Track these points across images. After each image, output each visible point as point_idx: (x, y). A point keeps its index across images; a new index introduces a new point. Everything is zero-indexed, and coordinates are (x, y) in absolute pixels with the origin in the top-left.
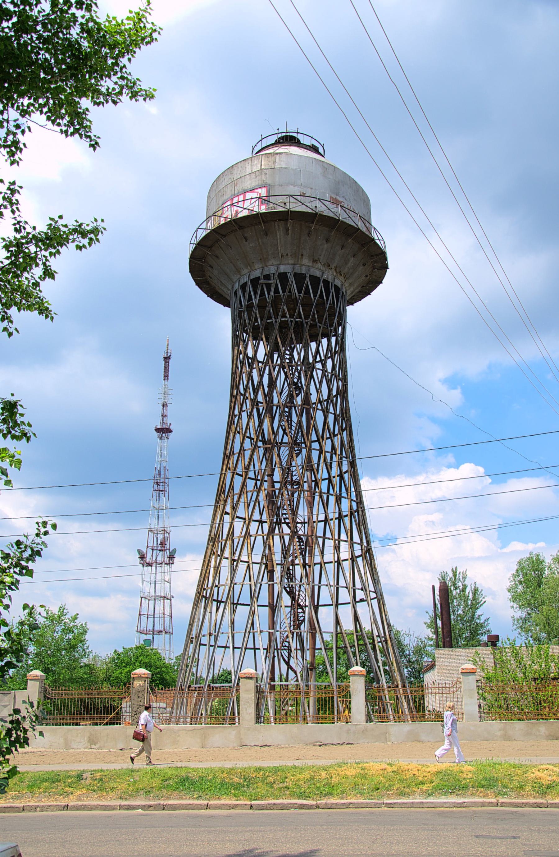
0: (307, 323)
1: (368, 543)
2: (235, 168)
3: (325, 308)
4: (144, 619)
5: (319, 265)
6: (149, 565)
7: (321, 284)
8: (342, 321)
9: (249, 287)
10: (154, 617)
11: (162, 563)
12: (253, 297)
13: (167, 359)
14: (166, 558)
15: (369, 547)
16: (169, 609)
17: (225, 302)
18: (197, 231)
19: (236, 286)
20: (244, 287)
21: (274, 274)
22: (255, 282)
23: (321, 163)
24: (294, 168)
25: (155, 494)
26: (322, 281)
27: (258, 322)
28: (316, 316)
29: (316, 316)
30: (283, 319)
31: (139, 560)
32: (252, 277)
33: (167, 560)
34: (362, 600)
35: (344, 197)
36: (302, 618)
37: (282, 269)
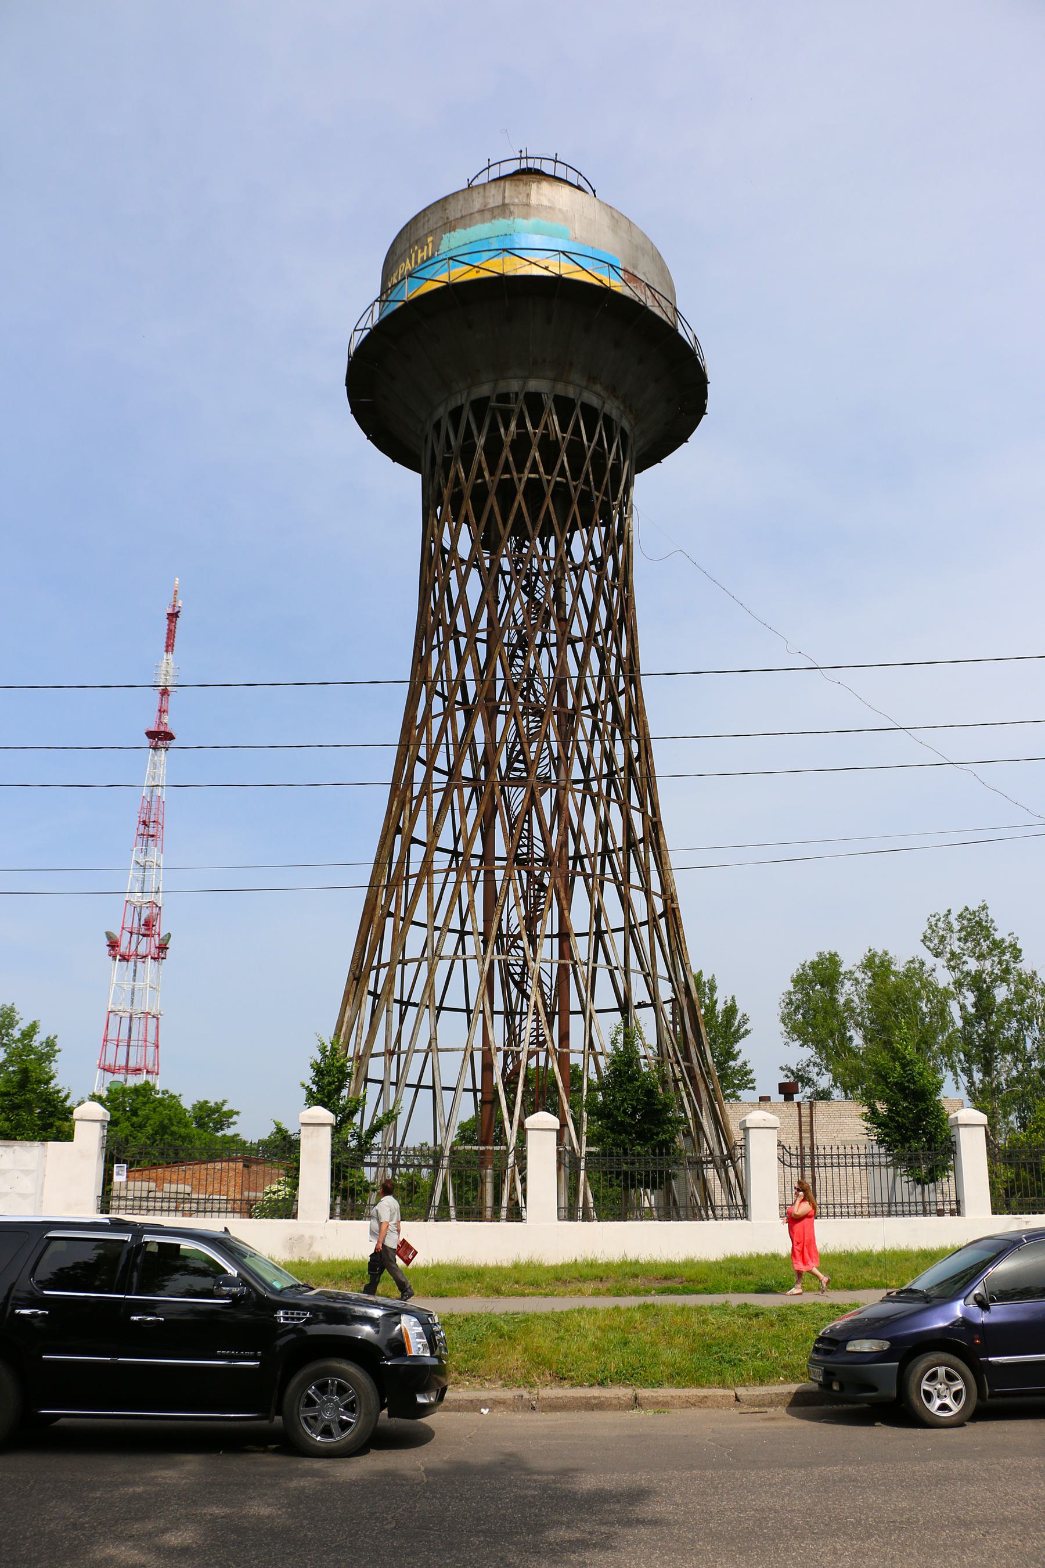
0: (575, 487)
2: (451, 199)
3: (606, 465)
4: (111, 1047)
5: (598, 388)
6: (125, 958)
9: (467, 414)
10: (129, 1046)
12: (475, 432)
13: (173, 616)
14: (153, 949)
16: (154, 1034)
19: (442, 412)
20: (456, 415)
21: (517, 394)
22: (479, 406)
23: (609, 209)
25: (140, 840)
30: (532, 476)
31: (108, 949)
32: (473, 397)
33: (154, 951)
37: (534, 385)
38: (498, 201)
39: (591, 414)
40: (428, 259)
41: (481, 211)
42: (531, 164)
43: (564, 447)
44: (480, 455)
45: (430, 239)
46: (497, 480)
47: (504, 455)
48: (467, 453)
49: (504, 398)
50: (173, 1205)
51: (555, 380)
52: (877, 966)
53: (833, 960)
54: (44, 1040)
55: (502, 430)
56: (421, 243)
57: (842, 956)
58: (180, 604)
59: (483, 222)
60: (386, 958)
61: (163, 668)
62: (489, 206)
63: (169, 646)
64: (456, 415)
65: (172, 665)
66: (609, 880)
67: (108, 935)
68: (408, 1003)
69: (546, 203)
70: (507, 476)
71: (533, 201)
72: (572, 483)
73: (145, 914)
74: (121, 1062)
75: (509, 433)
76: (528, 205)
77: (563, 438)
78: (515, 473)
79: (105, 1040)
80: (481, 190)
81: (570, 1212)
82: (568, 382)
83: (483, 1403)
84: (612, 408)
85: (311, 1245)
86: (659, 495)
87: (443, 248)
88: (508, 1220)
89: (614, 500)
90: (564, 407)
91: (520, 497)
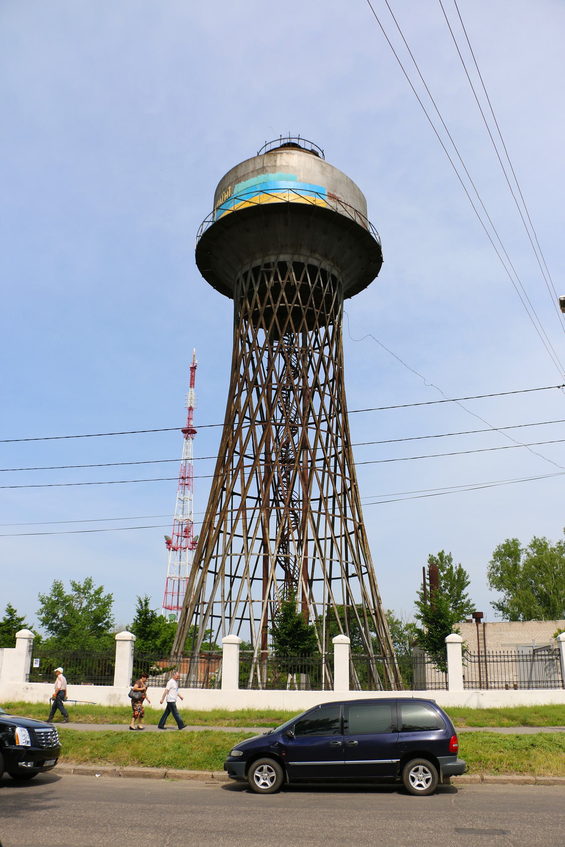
0: (304, 309)
1: (360, 520)
2: (239, 167)
3: (322, 295)
4: (169, 596)
5: (317, 256)
6: (175, 549)
7: (319, 273)
8: (337, 311)
9: (251, 275)
10: (178, 595)
11: (186, 548)
12: (254, 284)
13: (193, 369)
15: (361, 524)
17: (230, 295)
18: (202, 224)
19: (240, 275)
20: (245, 275)
21: (274, 263)
22: (256, 270)
24: (294, 166)
25: (181, 487)
26: (319, 270)
27: (258, 307)
28: (314, 302)
29: (314, 302)
30: (282, 305)
32: (253, 266)
34: (353, 575)
35: (341, 194)
36: (295, 591)
37: (283, 258)
38: (261, 166)
39: (313, 270)
40: (229, 198)
41: (253, 171)
42: (293, 141)
43: (298, 288)
44: (256, 296)
45: (230, 188)
46: (264, 308)
47: (267, 295)
48: (250, 294)
49: (268, 265)
50: (527, 685)
51: (293, 254)
52: (539, 546)
53: (515, 543)
54: (107, 595)
55: (267, 282)
56: (226, 190)
57: (520, 540)
58: (196, 362)
59: (253, 177)
60: (220, 553)
61: (189, 396)
62: (256, 168)
63: (192, 384)
64: (245, 275)
65: (194, 394)
66: (315, 512)
67: (166, 537)
68: (235, 577)
69: (284, 164)
70: (269, 306)
71: (278, 163)
72: (303, 307)
73: (184, 527)
74: (175, 604)
75: (270, 283)
76: (275, 166)
77: (298, 283)
78: (273, 304)
79: (166, 593)
80: (253, 161)
81: (243, 684)
82: (300, 255)
83: (98, 772)
84: (326, 265)
85: (119, 699)
86: (353, 307)
87: (235, 192)
88: (325, 690)
89: (328, 312)
90: (298, 267)
91: (304, 319)
